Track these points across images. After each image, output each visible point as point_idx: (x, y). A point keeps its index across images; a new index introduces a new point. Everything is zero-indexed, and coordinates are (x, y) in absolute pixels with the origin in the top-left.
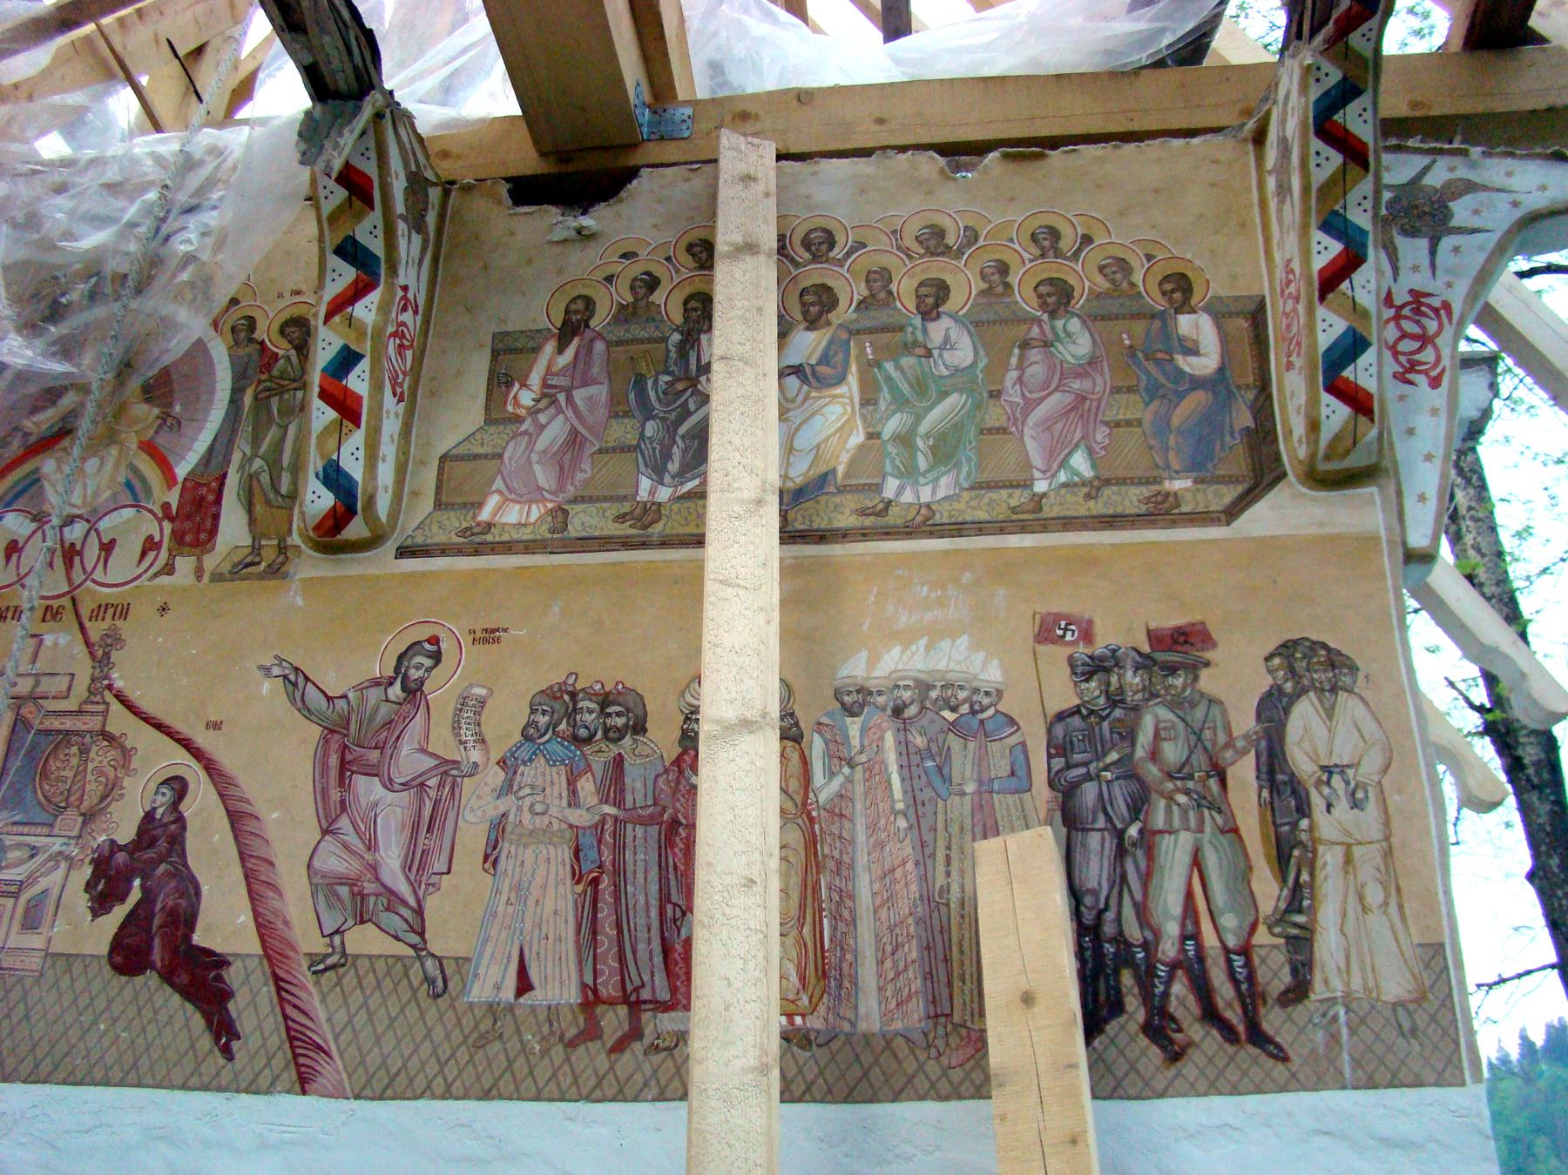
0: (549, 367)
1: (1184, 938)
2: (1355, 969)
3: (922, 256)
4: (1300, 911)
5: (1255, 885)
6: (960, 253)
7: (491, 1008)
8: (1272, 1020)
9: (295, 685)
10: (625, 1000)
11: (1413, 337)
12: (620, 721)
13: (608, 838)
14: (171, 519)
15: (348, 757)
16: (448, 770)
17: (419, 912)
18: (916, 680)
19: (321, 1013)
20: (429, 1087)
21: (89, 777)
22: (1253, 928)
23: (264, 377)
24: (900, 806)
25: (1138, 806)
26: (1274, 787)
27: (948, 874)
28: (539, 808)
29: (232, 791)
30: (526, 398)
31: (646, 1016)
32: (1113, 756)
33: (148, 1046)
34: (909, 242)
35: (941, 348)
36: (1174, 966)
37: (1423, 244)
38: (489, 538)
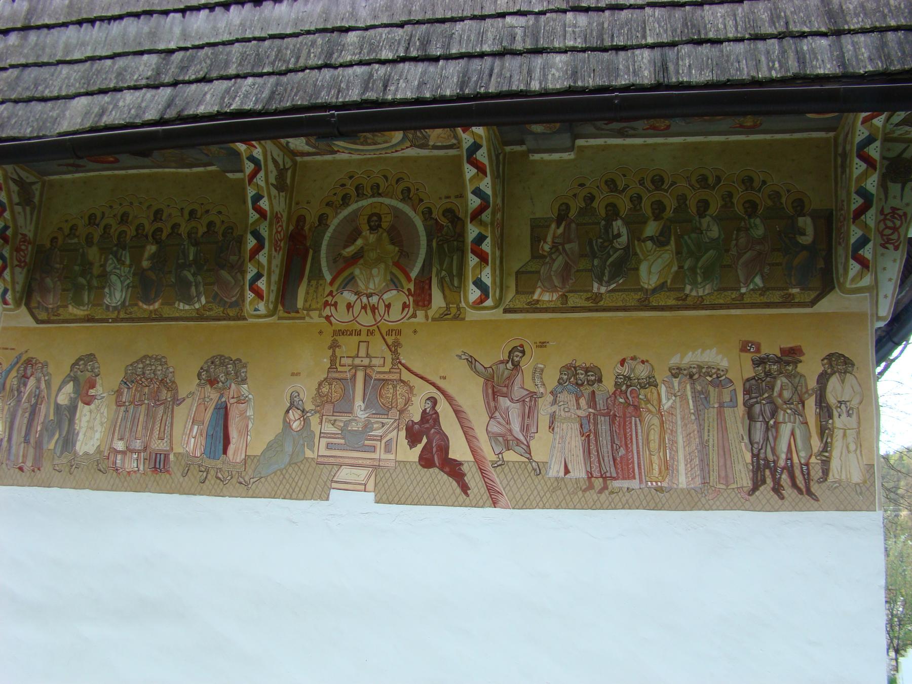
0: (554, 234)
1: (787, 459)
2: (844, 472)
3: (699, 189)
4: (827, 452)
5: (812, 442)
6: (714, 188)
7: (557, 479)
8: (814, 488)
9: (471, 362)
10: (601, 476)
11: (890, 228)
12: (593, 378)
13: (592, 420)
14: (412, 296)
15: (495, 390)
16: (533, 396)
17: (528, 446)
18: (698, 365)
19: (497, 481)
20: (537, 505)
21: (398, 397)
22: (810, 456)
23: (439, 235)
24: (692, 411)
25: (774, 414)
26: (821, 408)
27: (709, 436)
28: (567, 410)
29: (454, 402)
30: (547, 248)
31: (608, 482)
32: (766, 395)
33: (287, 482)
34: (693, 182)
35: (707, 230)
36: (783, 469)
37: (899, 186)
38: (538, 306)
